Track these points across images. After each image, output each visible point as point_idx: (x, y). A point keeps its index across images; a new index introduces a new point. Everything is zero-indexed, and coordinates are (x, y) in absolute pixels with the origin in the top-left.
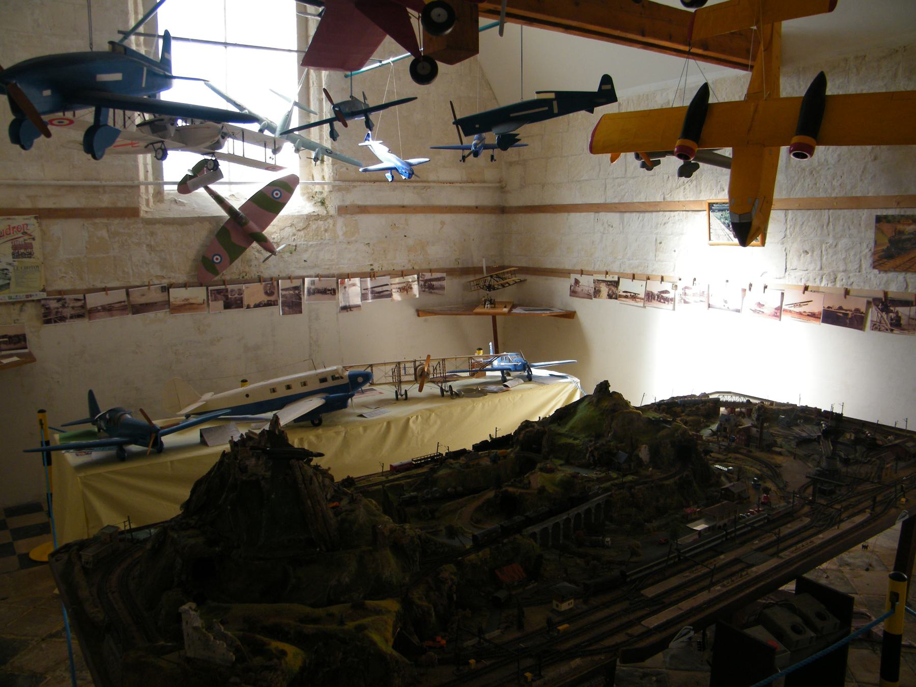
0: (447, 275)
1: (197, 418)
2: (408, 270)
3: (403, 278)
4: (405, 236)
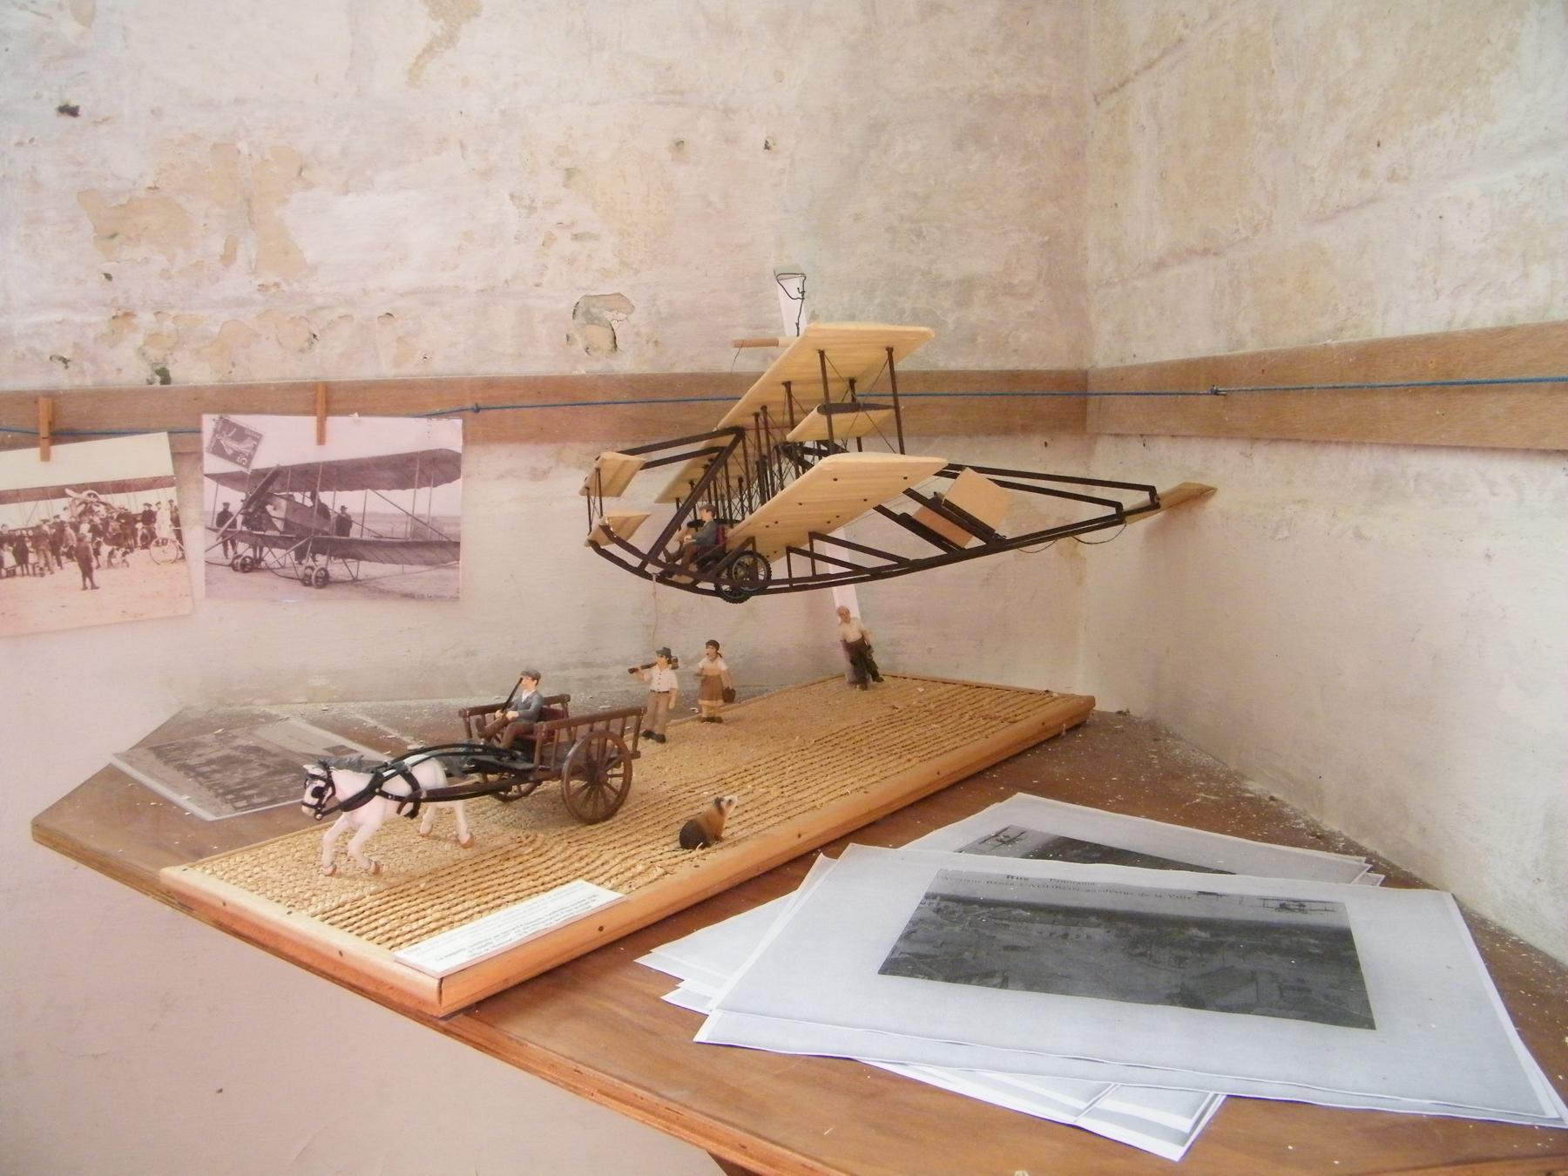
0: (468, 439)
1: (566, 772)
2: (103, 397)
3: (46, 457)
4: (70, 111)
